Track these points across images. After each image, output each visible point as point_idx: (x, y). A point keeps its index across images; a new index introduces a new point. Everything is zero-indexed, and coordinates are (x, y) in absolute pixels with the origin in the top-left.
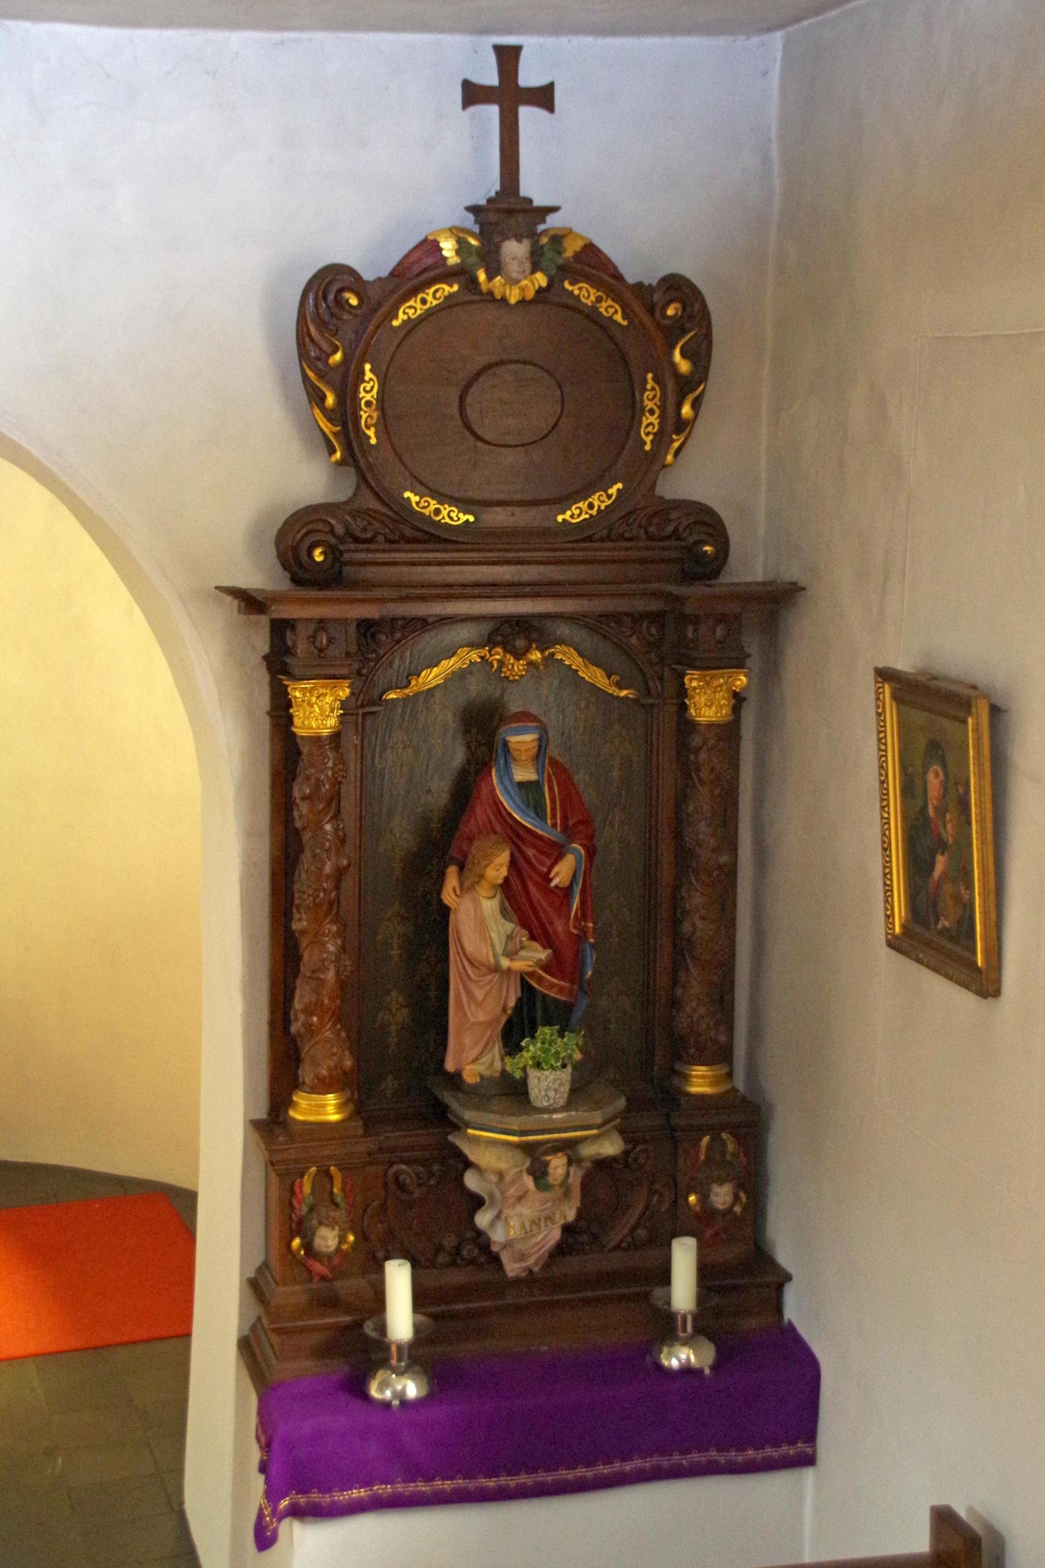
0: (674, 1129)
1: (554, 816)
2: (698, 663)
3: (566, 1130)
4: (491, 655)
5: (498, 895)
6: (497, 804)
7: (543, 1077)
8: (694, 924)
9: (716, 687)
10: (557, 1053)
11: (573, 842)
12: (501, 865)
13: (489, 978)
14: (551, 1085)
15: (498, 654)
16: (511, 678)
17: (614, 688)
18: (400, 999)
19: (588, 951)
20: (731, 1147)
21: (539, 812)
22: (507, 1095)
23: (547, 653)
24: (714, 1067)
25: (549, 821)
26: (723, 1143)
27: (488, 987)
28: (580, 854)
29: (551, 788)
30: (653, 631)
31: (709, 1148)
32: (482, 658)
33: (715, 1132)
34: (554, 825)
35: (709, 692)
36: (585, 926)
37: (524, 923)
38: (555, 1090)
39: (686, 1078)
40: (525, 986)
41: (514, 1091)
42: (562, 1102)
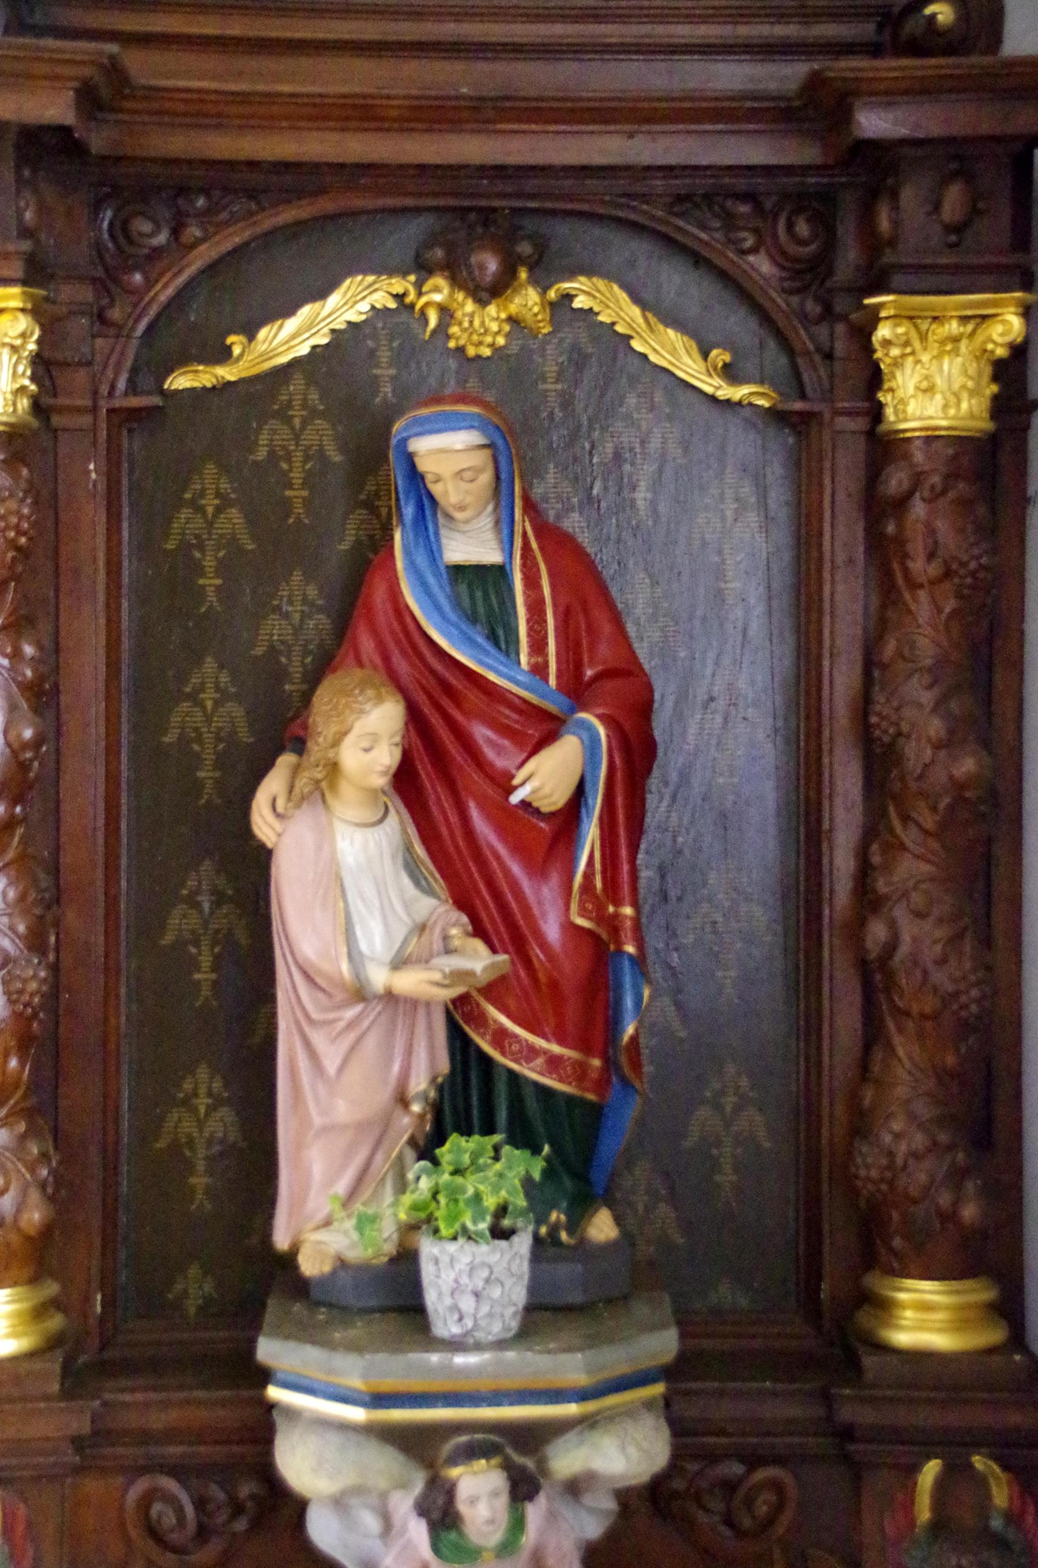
0: (847, 1433)
1: (538, 646)
2: (897, 280)
3: (496, 1398)
4: (420, 294)
5: (393, 820)
6: (401, 611)
7: (445, 1260)
8: (893, 926)
9: (943, 342)
10: (477, 1197)
11: (584, 708)
12: (375, 737)
13: (350, 1013)
14: (465, 1280)
15: (439, 291)
16: (471, 351)
17: (717, 381)
18: (217, 1085)
19: (627, 980)
20: (1001, 1496)
21: (499, 634)
22: (383, 1310)
23: (552, 294)
24: (955, 1285)
25: (524, 659)
26: (981, 1482)
27: (352, 1036)
28: (595, 739)
29: (531, 582)
30: (803, 228)
31: (941, 1485)
32: (399, 297)
33: (953, 1447)
34: (539, 670)
35: (925, 358)
36: (616, 916)
37: (463, 901)
38: (477, 1295)
39: (885, 1307)
40: (460, 1045)
41: (394, 1298)
42: (496, 1329)
